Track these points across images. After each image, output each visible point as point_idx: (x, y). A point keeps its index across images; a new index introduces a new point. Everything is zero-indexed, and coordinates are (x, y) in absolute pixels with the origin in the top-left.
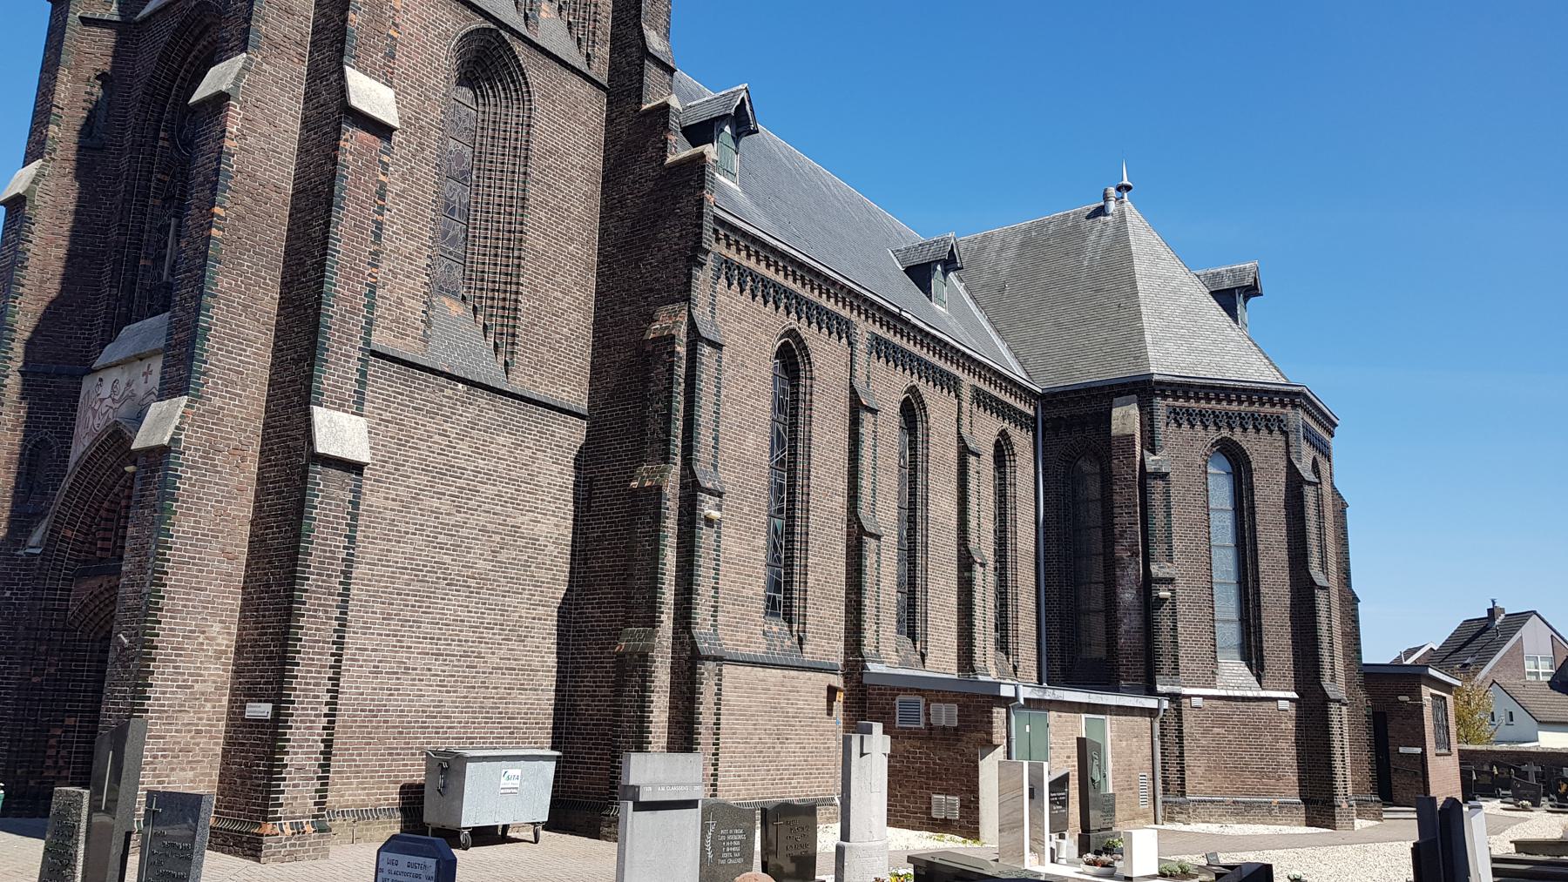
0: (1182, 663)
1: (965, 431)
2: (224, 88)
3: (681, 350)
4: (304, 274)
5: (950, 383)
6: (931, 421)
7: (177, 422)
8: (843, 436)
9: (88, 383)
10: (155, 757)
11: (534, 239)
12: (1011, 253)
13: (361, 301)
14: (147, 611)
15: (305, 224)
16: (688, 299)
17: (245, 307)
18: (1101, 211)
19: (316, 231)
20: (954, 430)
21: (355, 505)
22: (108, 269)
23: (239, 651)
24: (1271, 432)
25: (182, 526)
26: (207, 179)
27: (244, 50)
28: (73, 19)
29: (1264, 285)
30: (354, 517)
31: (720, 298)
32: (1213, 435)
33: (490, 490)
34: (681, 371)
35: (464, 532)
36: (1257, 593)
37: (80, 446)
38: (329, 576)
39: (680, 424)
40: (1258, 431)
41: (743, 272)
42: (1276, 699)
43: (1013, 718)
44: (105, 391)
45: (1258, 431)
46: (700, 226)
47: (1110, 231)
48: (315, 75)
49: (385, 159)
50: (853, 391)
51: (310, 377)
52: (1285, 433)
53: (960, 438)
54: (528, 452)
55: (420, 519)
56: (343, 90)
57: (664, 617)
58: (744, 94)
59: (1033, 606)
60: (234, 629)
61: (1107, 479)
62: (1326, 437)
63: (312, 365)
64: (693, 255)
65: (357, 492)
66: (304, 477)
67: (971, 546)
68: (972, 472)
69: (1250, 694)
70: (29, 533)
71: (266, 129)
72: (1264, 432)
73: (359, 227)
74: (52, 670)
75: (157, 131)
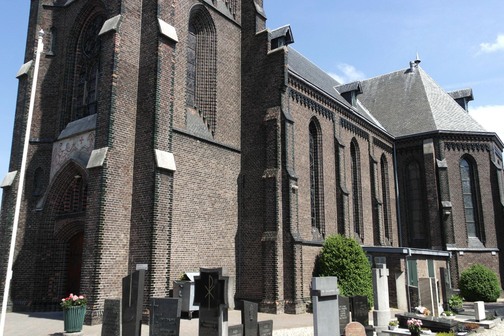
0: (456, 238)
1: (371, 154)
2: (114, 28)
3: (279, 124)
4: (147, 99)
5: (365, 136)
6: (360, 150)
7: (105, 157)
8: (333, 156)
9: (56, 146)
10: (105, 286)
11: (219, 84)
12: (375, 88)
13: (169, 108)
14: (98, 228)
15: (146, 80)
16: (280, 105)
17: (125, 112)
18: (409, 71)
19: (151, 82)
20: (368, 153)
21: (172, 187)
22: (60, 101)
23: (131, 244)
24: (483, 151)
25: (109, 197)
26: (108, 63)
27: (119, 13)
28: (41, 5)
29: (474, 96)
30: (172, 192)
31: (291, 104)
32: (462, 153)
33: (210, 181)
34: (279, 132)
35: (202, 197)
36: (482, 211)
37: (55, 169)
38: (165, 214)
39: (280, 153)
40: (478, 151)
41: (298, 94)
42: (490, 252)
43: (407, 262)
44: (64, 147)
45: (478, 151)
46: (284, 77)
47: (413, 78)
48: (145, 23)
49: (174, 54)
50: (336, 139)
51: (153, 138)
52: (488, 151)
53: (370, 157)
54: (222, 166)
55: (188, 192)
56: (158, 27)
57: (279, 227)
58: (288, 28)
59: (396, 220)
60: (129, 236)
61: (422, 171)
62: (500, 152)
63: (153, 134)
64: (282, 89)
65: (172, 182)
66: (154, 177)
67: (377, 197)
68: (375, 170)
69: (481, 249)
70: (36, 203)
71: (129, 44)
72: (481, 151)
73: (166, 80)
74: (49, 255)
75: (76, 48)
